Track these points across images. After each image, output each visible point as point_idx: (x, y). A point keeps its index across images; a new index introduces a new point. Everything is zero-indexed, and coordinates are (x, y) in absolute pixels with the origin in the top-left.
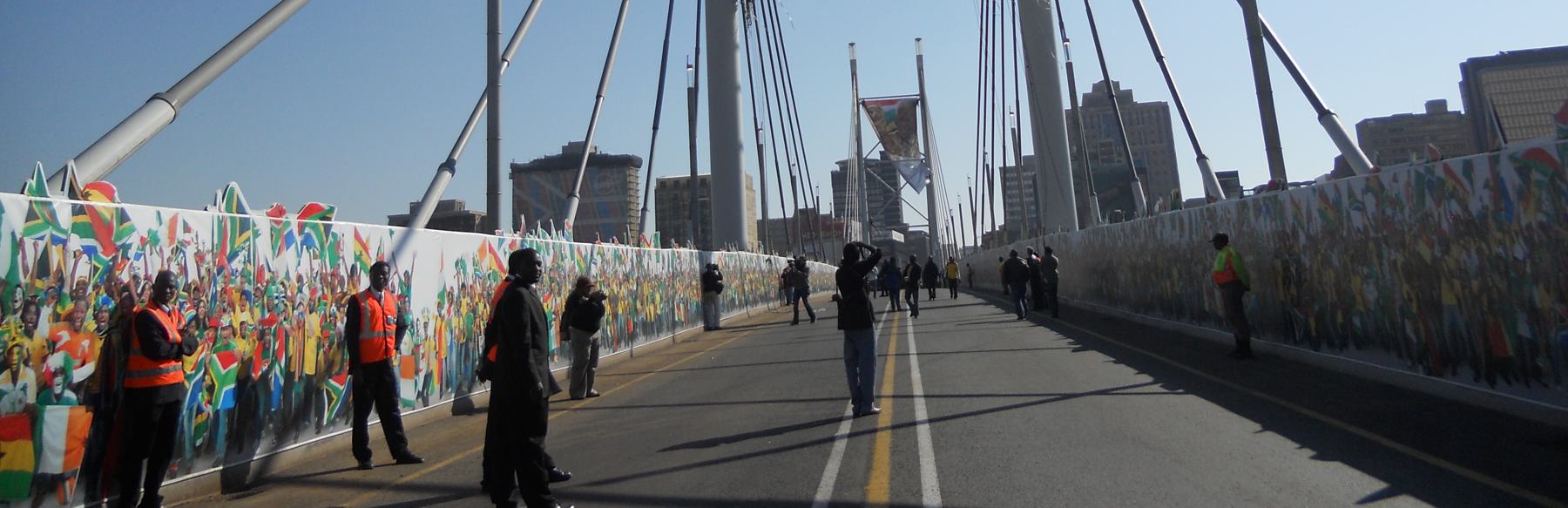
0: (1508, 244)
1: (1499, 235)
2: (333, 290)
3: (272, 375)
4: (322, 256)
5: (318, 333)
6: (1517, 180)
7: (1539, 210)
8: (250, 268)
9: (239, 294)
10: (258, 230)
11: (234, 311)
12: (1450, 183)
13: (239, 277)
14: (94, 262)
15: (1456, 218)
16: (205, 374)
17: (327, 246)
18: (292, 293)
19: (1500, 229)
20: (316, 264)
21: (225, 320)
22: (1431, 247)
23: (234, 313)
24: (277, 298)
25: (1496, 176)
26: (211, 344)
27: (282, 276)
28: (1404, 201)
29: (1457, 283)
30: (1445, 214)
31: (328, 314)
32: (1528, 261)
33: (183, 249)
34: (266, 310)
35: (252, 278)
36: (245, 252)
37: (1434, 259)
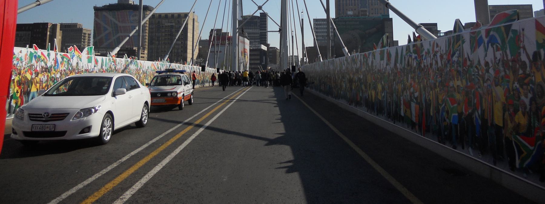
0: (56, 74)
1: (54, 72)
2: (515, 72)
3: (474, 116)
4: (503, 48)
5: (503, 99)
6: (61, 60)
7: (64, 67)
8: (461, 59)
9: (456, 72)
10: (464, 40)
11: (454, 80)
12: (42, 57)
13: (456, 64)
14: (417, 61)
15: (42, 67)
16: (445, 105)
17: (507, 41)
18: (482, 72)
19: (55, 70)
20: (499, 54)
21: (451, 84)
22: (31, 74)
23: (454, 81)
24: (474, 75)
25: (56, 58)
26: (447, 93)
27: (476, 62)
28: (24, 59)
29: (38, 85)
30: (38, 66)
31: (511, 88)
32: (60, 78)
33: (436, 54)
34: (468, 81)
35: (461, 64)
36: (458, 52)
37: (32, 78)
